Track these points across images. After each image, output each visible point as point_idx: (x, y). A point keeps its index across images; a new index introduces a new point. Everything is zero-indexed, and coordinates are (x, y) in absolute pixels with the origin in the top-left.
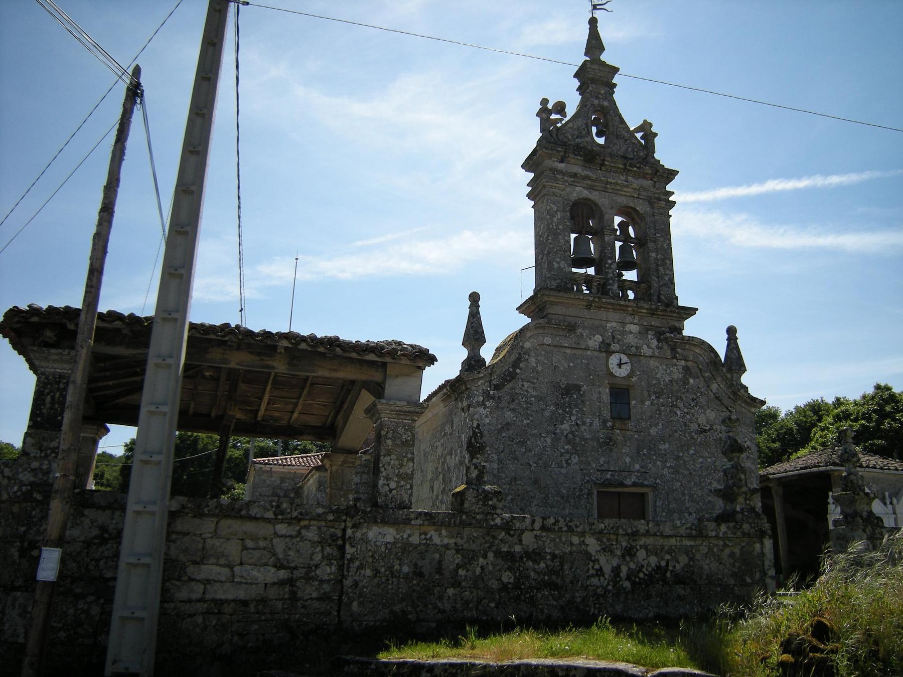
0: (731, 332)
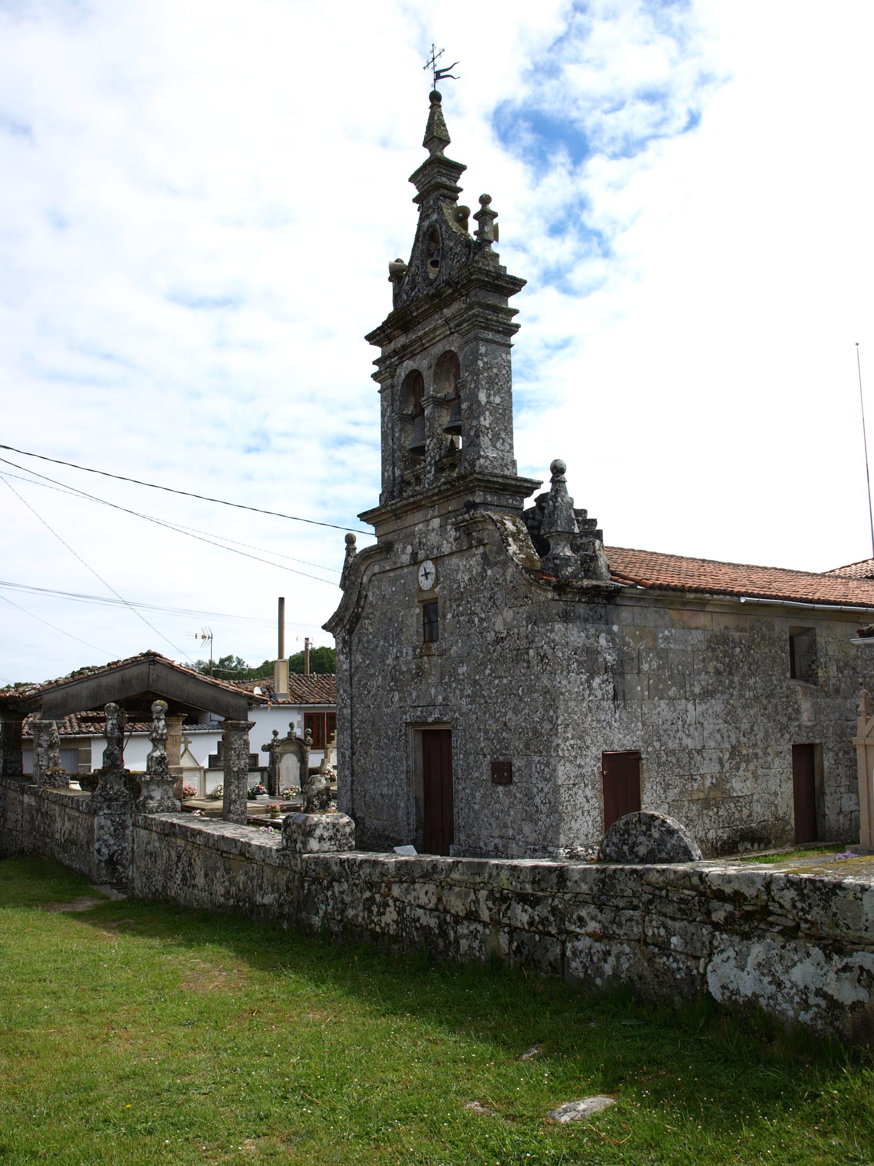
0: (558, 470)
